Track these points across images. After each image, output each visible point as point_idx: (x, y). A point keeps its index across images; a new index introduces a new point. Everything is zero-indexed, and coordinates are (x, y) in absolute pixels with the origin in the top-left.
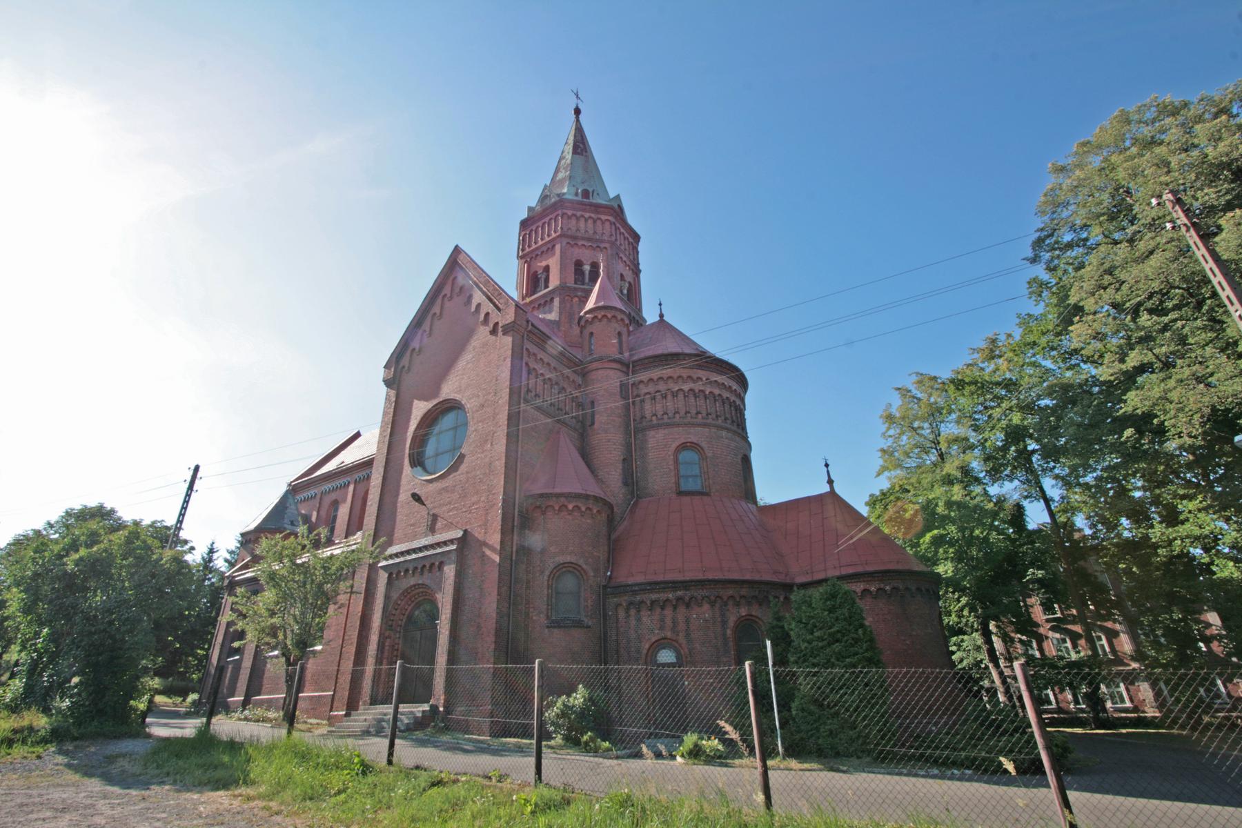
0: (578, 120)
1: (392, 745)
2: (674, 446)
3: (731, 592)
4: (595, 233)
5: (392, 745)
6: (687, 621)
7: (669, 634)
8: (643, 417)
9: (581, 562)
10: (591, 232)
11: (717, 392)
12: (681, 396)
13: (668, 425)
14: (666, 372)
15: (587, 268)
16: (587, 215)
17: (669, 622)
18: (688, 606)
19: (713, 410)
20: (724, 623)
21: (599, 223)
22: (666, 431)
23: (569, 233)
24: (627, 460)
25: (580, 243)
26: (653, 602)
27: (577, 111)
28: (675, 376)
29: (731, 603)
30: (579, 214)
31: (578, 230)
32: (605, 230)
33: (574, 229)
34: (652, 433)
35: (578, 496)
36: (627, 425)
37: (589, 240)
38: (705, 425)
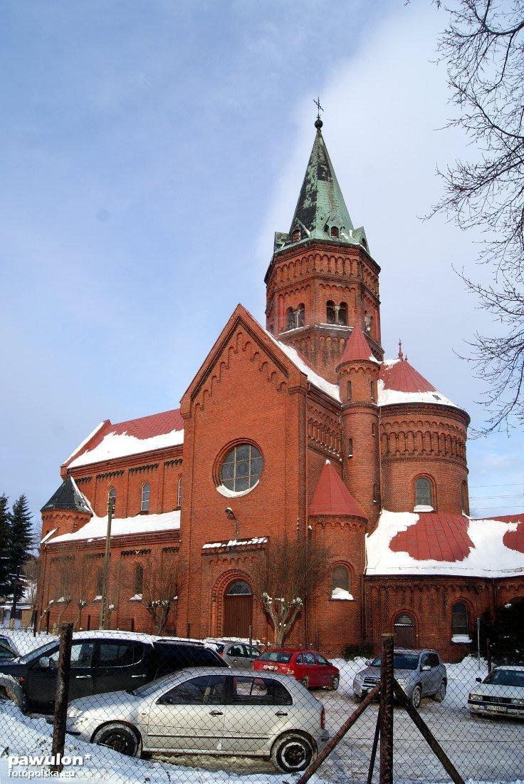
0: (319, 135)
1: (345, 729)
2: (412, 476)
3: (450, 583)
4: (344, 273)
5: (345, 729)
6: (421, 601)
7: (408, 607)
8: (388, 452)
9: (349, 561)
10: (341, 273)
11: (447, 433)
12: (419, 436)
13: (409, 459)
14: (423, 418)
15: (337, 308)
16: (337, 255)
17: (408, 600)
18: (421, 590)
19: (442, 448)
20: (444, 602)
21: (333, 260)
22: (407, 464)
23: (337, 277)
24: (377, 486)
25: (331, 284)
26: (397, 587)
27: (319, 125)
28: (416, 420)
29: (450, 589)
30: (329, 254)
31: (344, 273)
32: (352, 269)
33: (326, 270)
34: (396, 464)
35: (347, 517)
36: (377, 458)
37: (339, 281)
38: (437, 460)
